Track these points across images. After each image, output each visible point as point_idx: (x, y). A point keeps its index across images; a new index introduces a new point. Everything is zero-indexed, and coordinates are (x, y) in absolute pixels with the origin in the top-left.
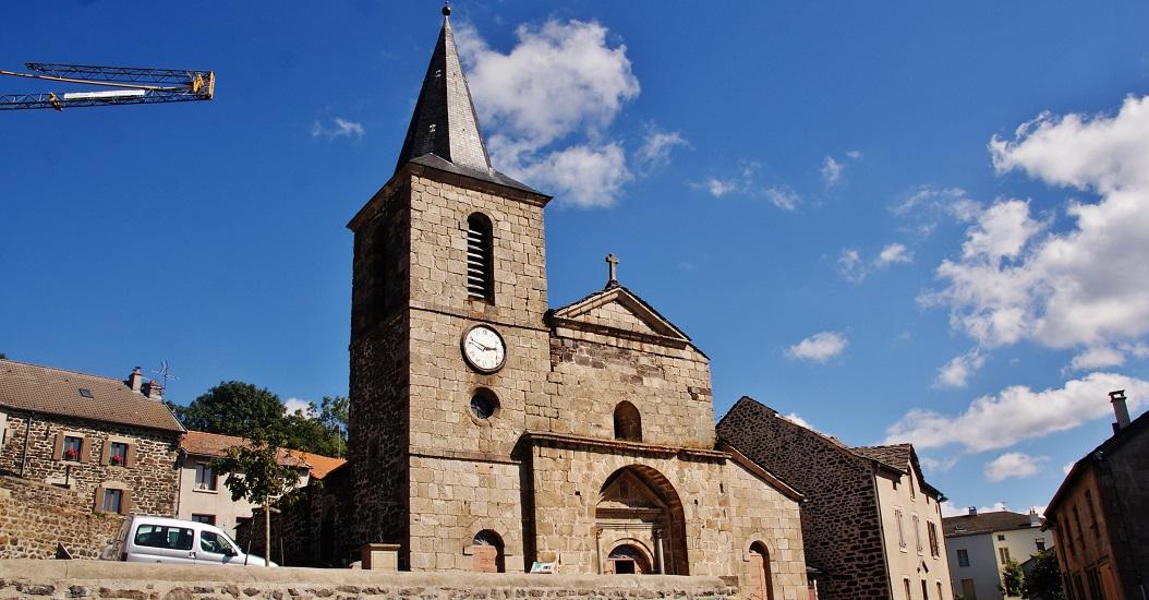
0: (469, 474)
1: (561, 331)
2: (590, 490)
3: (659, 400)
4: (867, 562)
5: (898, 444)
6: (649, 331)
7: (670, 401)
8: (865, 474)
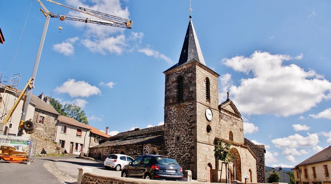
1: (222, 111)
4: (260, 175)
5: (261, 145)
6: (234, 113)
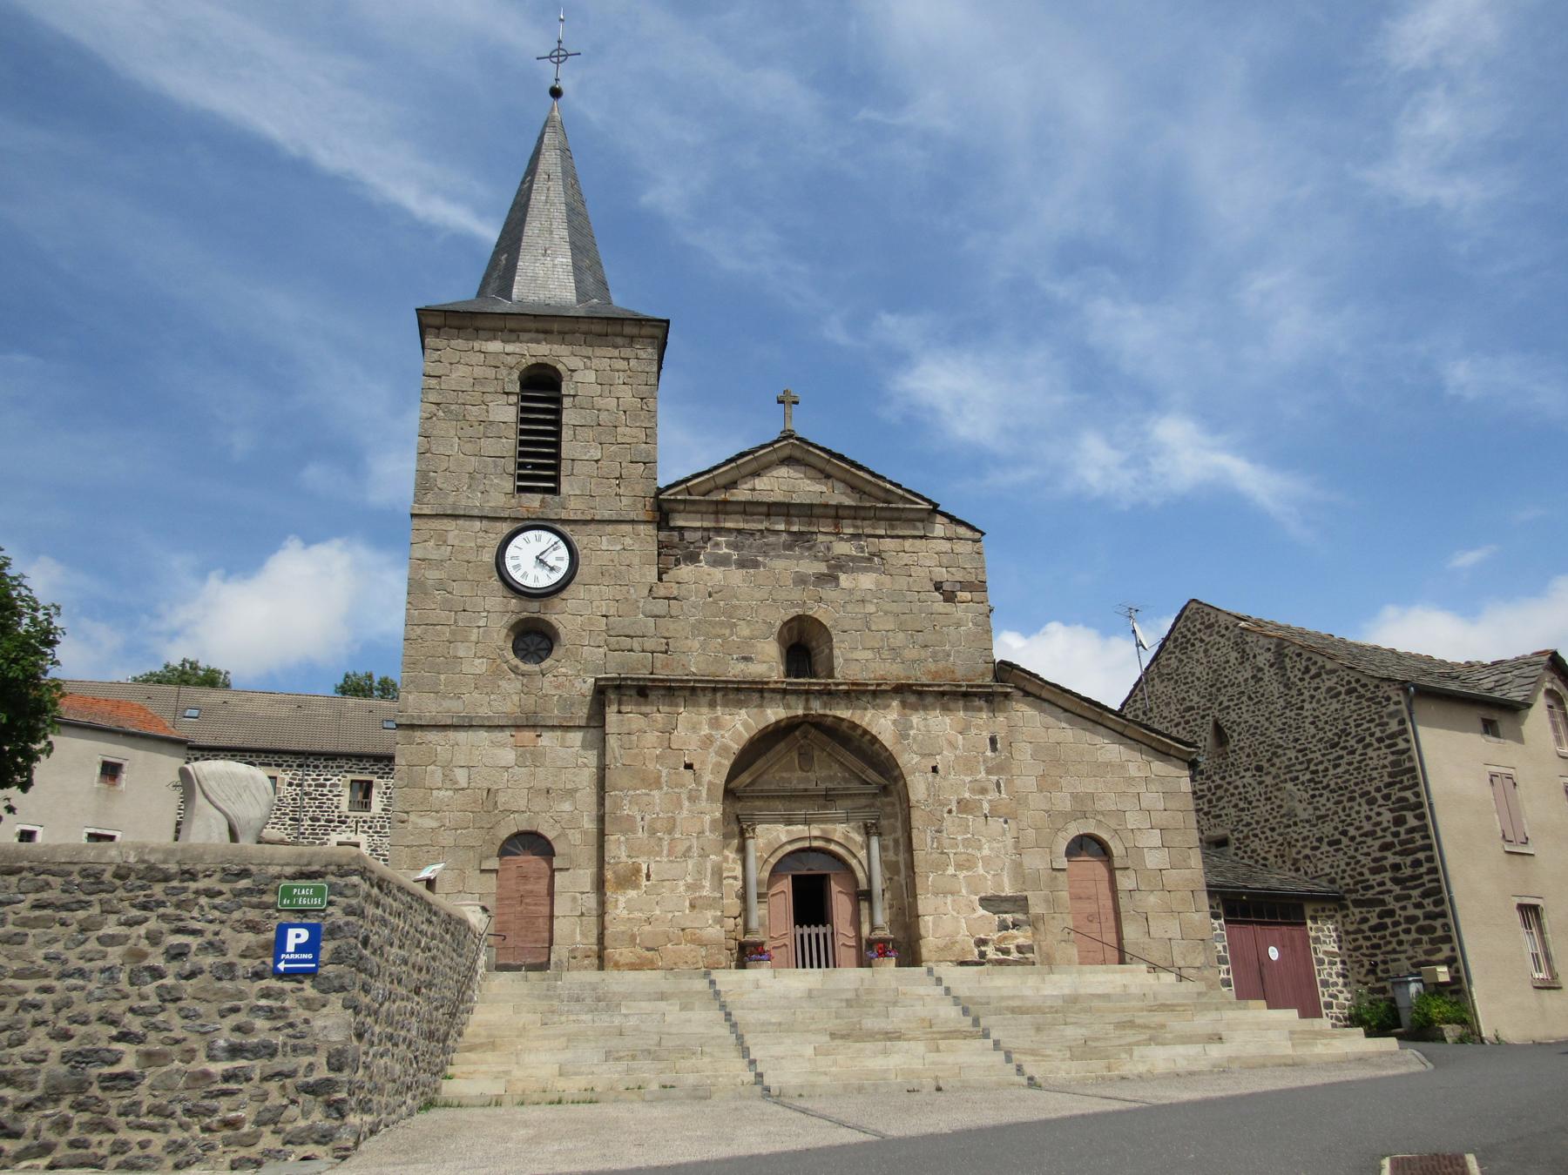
0: (500, 751)
2: (712, 758)
3: (871, 608)
4: (1408, 872)
7: (894, 607)
8: (1392, 707)
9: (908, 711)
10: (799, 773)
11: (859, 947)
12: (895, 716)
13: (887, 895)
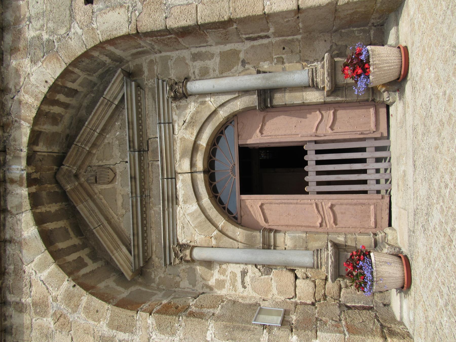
9: (21, 45)
10: (117, 183)
11: (336, 106)
12: (26, 62)
13: (265, 66)
